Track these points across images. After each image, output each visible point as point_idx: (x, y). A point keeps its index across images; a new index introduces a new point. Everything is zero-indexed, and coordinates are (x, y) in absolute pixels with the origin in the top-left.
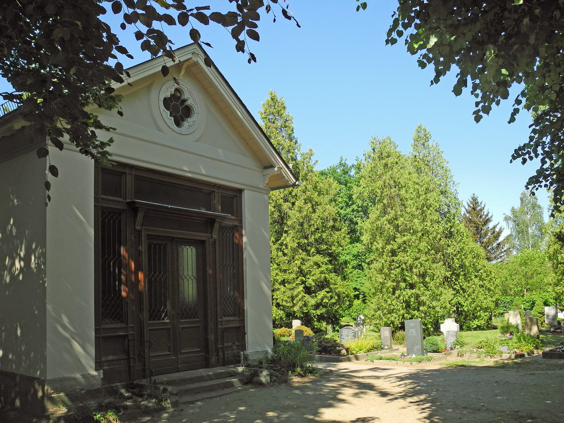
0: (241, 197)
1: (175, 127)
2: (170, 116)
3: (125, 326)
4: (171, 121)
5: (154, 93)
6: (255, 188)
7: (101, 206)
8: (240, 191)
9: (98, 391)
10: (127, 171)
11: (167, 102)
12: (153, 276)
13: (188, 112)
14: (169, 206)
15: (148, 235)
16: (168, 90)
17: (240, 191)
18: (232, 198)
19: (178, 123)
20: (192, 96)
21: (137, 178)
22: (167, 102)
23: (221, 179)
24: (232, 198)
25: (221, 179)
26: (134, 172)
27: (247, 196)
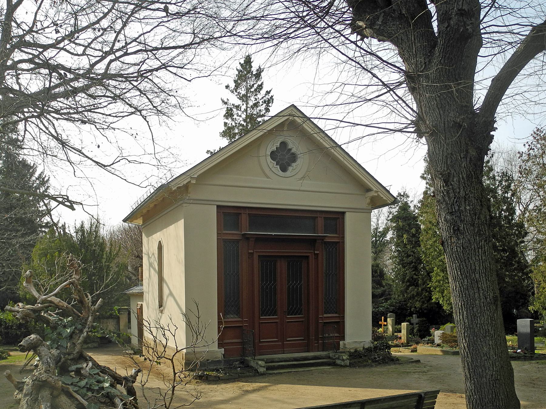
0: (344, 218)
1: (281, 173)
2: (277, 165)
3: (241, 320)
4: (277, 169)
5: (262, 152)
6: (355, 210)
7: (223, 239)
8: (343, 213)
9: (219, 362)
10: (242, 212)
11: (273, 155)
12: (291, 284)
13: (293, 158)
14: (273, 234)
15: (259, 256)
16: (273, 145)
17: (343, 213)
18: (335, 220)
19: (284, 169)
20: (295, 145)
21: (325, 218)
22: (273, 155)
23: (332, 207)
24: (335, 220)
25: (332, 207)
26: (247, 212)
27: (348, 217)
